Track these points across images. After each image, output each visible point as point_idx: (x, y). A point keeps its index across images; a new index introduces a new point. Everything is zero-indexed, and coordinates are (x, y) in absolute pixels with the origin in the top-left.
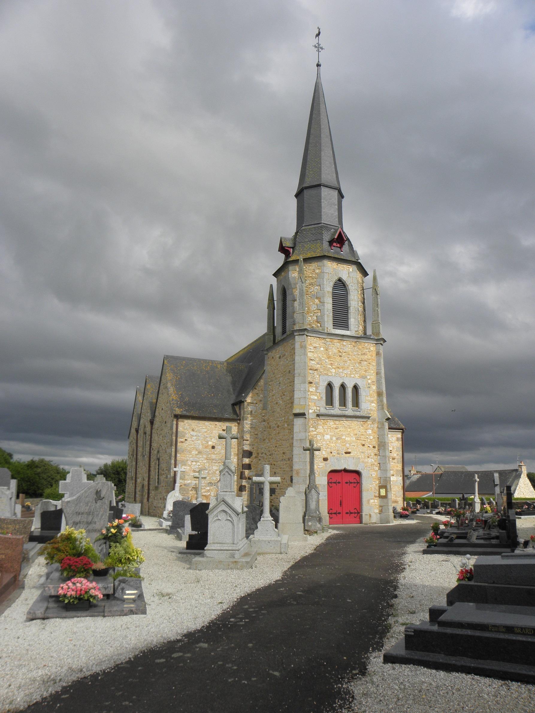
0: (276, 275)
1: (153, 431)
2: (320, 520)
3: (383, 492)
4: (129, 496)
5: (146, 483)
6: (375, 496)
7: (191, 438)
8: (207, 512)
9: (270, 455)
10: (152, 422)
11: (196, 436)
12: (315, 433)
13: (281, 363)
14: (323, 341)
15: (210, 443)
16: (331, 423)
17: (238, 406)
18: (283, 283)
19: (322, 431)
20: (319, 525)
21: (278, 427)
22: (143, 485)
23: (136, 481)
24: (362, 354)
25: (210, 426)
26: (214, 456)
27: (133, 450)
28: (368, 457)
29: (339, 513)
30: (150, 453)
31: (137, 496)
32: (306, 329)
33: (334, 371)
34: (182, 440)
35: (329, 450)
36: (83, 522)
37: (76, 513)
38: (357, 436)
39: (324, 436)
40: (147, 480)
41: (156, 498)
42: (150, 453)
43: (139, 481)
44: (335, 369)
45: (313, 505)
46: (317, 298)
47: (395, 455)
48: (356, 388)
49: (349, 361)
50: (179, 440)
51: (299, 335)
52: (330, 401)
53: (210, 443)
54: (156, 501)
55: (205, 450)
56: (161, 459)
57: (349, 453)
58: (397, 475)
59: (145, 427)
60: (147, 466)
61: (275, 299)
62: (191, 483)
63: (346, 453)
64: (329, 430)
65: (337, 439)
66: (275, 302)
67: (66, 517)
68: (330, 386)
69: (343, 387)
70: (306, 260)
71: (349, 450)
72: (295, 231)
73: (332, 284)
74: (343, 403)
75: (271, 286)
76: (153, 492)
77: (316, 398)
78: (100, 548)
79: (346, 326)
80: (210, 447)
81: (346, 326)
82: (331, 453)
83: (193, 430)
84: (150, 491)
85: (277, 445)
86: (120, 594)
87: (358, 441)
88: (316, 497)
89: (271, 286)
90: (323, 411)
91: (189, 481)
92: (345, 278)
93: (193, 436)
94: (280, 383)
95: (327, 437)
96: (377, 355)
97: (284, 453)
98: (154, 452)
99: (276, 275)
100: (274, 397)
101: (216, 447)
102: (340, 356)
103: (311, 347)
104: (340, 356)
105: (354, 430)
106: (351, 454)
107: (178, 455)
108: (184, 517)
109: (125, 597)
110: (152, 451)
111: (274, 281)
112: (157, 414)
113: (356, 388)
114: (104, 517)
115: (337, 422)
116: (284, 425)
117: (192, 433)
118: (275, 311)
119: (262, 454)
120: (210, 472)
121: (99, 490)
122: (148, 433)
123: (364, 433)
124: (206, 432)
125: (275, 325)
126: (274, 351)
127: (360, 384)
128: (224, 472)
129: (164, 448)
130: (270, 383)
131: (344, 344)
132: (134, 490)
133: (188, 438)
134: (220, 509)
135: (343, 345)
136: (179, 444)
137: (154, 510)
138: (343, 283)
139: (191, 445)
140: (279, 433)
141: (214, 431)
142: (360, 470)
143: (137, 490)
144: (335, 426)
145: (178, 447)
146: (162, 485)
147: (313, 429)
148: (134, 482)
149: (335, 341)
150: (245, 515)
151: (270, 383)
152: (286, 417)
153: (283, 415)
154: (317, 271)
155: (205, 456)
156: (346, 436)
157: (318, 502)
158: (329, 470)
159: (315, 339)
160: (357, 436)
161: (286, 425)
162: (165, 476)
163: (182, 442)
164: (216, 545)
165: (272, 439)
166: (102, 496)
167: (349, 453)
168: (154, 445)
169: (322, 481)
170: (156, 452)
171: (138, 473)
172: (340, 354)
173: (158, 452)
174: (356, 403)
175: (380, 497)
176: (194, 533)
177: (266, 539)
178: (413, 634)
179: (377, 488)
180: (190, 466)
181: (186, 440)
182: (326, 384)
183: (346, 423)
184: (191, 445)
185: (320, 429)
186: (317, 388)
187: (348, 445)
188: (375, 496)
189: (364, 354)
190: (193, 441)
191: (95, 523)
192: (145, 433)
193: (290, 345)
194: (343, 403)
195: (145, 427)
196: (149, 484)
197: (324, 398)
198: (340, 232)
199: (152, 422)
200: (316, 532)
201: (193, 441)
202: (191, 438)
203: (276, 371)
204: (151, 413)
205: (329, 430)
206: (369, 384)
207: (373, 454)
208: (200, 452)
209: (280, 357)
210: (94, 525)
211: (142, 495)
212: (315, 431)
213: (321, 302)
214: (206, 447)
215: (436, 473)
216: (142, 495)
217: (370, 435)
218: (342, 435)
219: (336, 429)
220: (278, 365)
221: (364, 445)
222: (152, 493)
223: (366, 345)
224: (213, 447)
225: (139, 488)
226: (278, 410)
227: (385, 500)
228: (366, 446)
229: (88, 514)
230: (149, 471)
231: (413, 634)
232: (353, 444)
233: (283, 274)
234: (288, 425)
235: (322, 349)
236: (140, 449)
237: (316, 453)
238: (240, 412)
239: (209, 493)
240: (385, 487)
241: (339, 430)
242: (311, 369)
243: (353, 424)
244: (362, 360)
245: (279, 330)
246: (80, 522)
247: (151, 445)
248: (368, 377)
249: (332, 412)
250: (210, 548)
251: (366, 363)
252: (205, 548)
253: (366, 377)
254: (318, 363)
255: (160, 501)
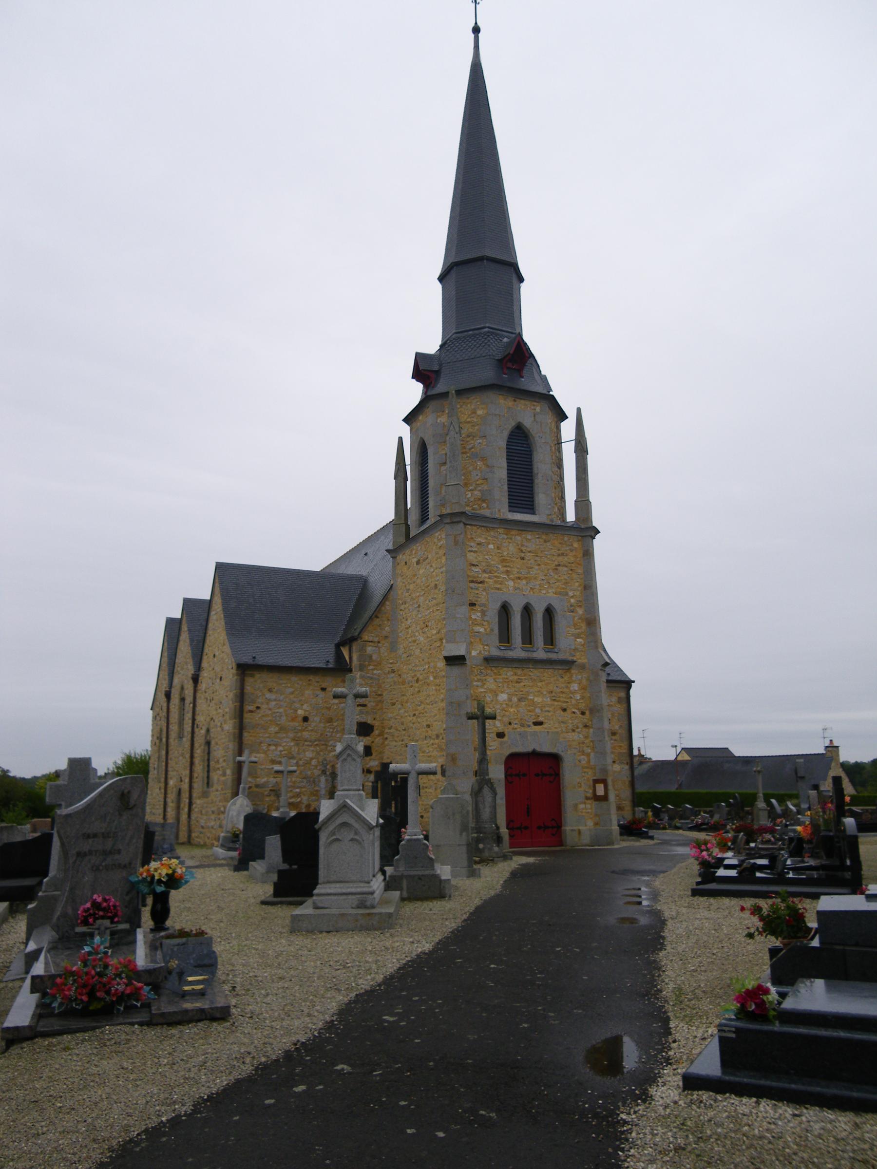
0: (407, 420)
1: (198, 695)
2: (499, 840)
3: (600, 790)
4: (154, 811)
5: (185, 786)
6: (587, 798)
7: (268, 704)
8: (317, 827)
9: (405, 730)
10: (196, 679)
11: (275, 700)
12: (482, 690)
13: (421, 572)
14: (492, 533)
15: (300, 712)
16: (508, 673)
17: (347, 648)
18: (421, 435)
19: (493, 686)
20: (496, 849)
21: (417, 681)
22: (180, 790)
23: (166, 783)
24: (559, 555)
25: (301, 683)
26: (306, 734)
27: (161, 730)
28: (574, 731)
29: (526, 828)
30: (193, 732)
31: (169, 809)
32: (463, 513)
33: (511, 583)
34: (250, 708)
35: (506, 719)
36: (96, 851)
37: (84, 835)
38: (554, 694)
39: (497, 695)
40: (187, 780)
41: (204, 812)
42: (193, 732)
43: (171, 783)
44: (513, 580)
45: (486, 813)
46: (483, 459)
47: (617, 727)
48: (549, 612)
49: (537, 567)
50: (248, 708)
51: (452, 523)
52: (505, 636)
53: (300, 712)
54: (205, 817)
55: (292, 724)
56: (213, 743)
57: (541, 723)
58: (621, 763)
59: (182, 688)
60: (188, 756)
61: (408, 461)
62: (267, 782)
63: (536, 724)
64: (506, 685)
65: (520, 700)
66: (408, 468)
67: (63, 844)
68: (505, 610)
69: (527, 610)
70: (460, 393)
71: (541, 719)
72: (440, 343)
73: (506, 434)
74: (528, 638)
75: (400, 439)
76: (198, 802)
77: (482, 630)
78: (127, 898)
79: (530, 508)
80: (300, 719)
81: (530, 508)
82: (510, 724)
83: (270, 690)
84: (194, 800)
85: (417, 713)
86: (177, 983)
87: (556, 703)
88: (490, 800)
89: (400, 439)
90: (495, 652)
91: (265, 779)
92: (527, 422)
93: (270, 700)
94: (419, 606)
95: (503, 697)
96: (584, 555)
97: (428, 726)
98: (200, 733)
99: (407, 420)
100: (410, 630)
101: (311, 719)
102: (522, 558)
103: (472, 544)
104: (522, 558)
105: (547, 684)
106: (544, 726)
107: (245, 734)
108: (263, 842)
109: (186, 988)
110: (196, 730)
111: (405, 431)
112: (204, 664)
113: (549, 612)
114: (134, 841)
115: (519, 672)
116: (428, 677)
117: (268, 695)
118: (409, 483)
119: (390, 728)
120: (301, 763)
121: (126, 791)
122: (189, 699)
123: (565, 690)
124: (292, 693)
125: (409, 506)
126: (408, 552)
127: (557, 605)
128: (344, 756)
129: (219, 724)
130: (402, 607)
131: (529, 537)
132: (162, 800)
133: (262, 703)
134: (339, 821)
135: (527, 539)
136: (246, 715)
137: (201, 833)
138: (524, 432)
139: (267, 715)
140: (419, 691)
141: (307, 692)
142: (562, 754)
143: (169, 800)
144: (516, 677)
145: (246, 721)
146: (216, 787)
147: (479, 684)
148: (162, 785)
149: (513, 532)
150: (377, 832)
151: (402, 607)
152: (432, 664)
153: (426, 660)
154: (480, 412)
155: (291, 735)
156: (535, 696)
157: (494, 807)
158: (508, 753)
159: (479, 531)
160: (554, 694)
161: (431, 678)
162: (220, 772)
163: (251, 711)
164: (333, 885)
165: (407, 702)
166: (132, 802)
167: (541, 723)
168: (200, 718)
169: (497, 772)
170: (203, 732)
171: (170, 769)
172: (523, 555)
173: (208, 731)
174: (550, 639)
175: (596, 798)
176: (286, 867)
177: (415, 873)
178: (733, 1035)
179: (591, 783)
180: (265, 753)
181: (258, 708)
182: (498, 605)
183: (535, 673)
184: (267, 715)
185: (491, 684)
186: (483, 613)
187: (538, 711)
188: (587, 798)
189: (563, 554)
190: (270, 709)
191: (119, 852)
192: (183, 700)
193: (436, 540)
194: (528, 638)
195: (182, 688)
196: (191, 787)
197: (496, 631)
198: (519, 342)
199: (196, 679)
200: (492, 860)
201: (270, 709)
202: (268, 704)
203: (411, 587)
204: (194, 665)
205: (506, 685)
206: (571, 606)
207: (581, 726)
208: (282, 729)
209: (418, 563)
210: (117, 857)
211: (178, 808)
212: (482, 687)
213: (488, 466)
214: (293, 720)
215: (679, 758)
216: (178, 808)
217: (575, 692)
218: (528, 693)
219: (517, 682)
220: (415, 575)
221: (564, 710)
222: (198, 802)
223: (566, 539)
224: (306, 719)
225: (172, 797)
226: (417, 652)
227: (603, 804)
228: (568, 711)
229: (106, 836)
230: (192, 764)
231: (733, 1035)
232: (547, 709)
233: (421, 418)
234: (435, 678)
235: (491, 546)
236: (174, 728)
237: (488, 723)
238: (351, 658)
239: (299, 800)
240: (604, 782)
241: (522, 684)
242: (472, 582)
243: (545, 674)
244: (559, 565)
245: (413, 518)
246: (90, 852)
247: (194, 720)
248: (571, 594)
249: (511, 654)
250: (323, 891)
251: (565, 569)
252: (315, 892)
253: (567, 594)
254: (484, 571)
255: (213, 817)
